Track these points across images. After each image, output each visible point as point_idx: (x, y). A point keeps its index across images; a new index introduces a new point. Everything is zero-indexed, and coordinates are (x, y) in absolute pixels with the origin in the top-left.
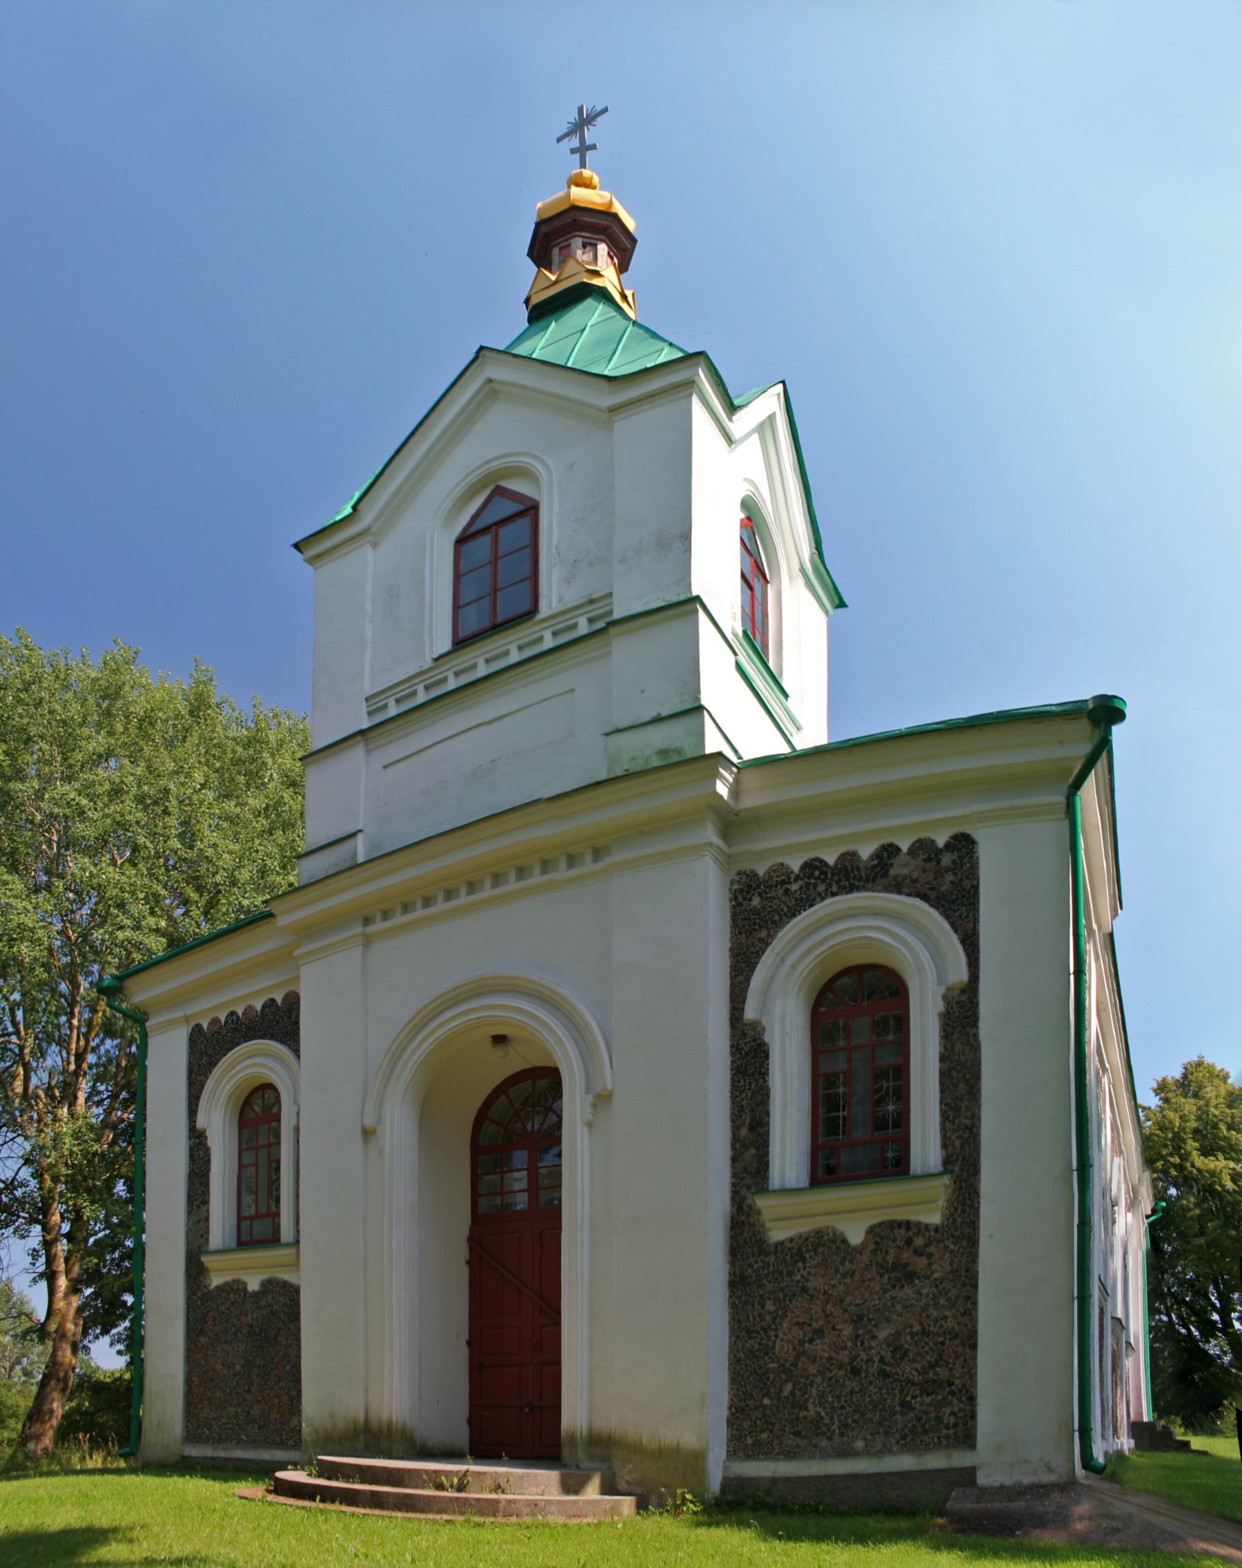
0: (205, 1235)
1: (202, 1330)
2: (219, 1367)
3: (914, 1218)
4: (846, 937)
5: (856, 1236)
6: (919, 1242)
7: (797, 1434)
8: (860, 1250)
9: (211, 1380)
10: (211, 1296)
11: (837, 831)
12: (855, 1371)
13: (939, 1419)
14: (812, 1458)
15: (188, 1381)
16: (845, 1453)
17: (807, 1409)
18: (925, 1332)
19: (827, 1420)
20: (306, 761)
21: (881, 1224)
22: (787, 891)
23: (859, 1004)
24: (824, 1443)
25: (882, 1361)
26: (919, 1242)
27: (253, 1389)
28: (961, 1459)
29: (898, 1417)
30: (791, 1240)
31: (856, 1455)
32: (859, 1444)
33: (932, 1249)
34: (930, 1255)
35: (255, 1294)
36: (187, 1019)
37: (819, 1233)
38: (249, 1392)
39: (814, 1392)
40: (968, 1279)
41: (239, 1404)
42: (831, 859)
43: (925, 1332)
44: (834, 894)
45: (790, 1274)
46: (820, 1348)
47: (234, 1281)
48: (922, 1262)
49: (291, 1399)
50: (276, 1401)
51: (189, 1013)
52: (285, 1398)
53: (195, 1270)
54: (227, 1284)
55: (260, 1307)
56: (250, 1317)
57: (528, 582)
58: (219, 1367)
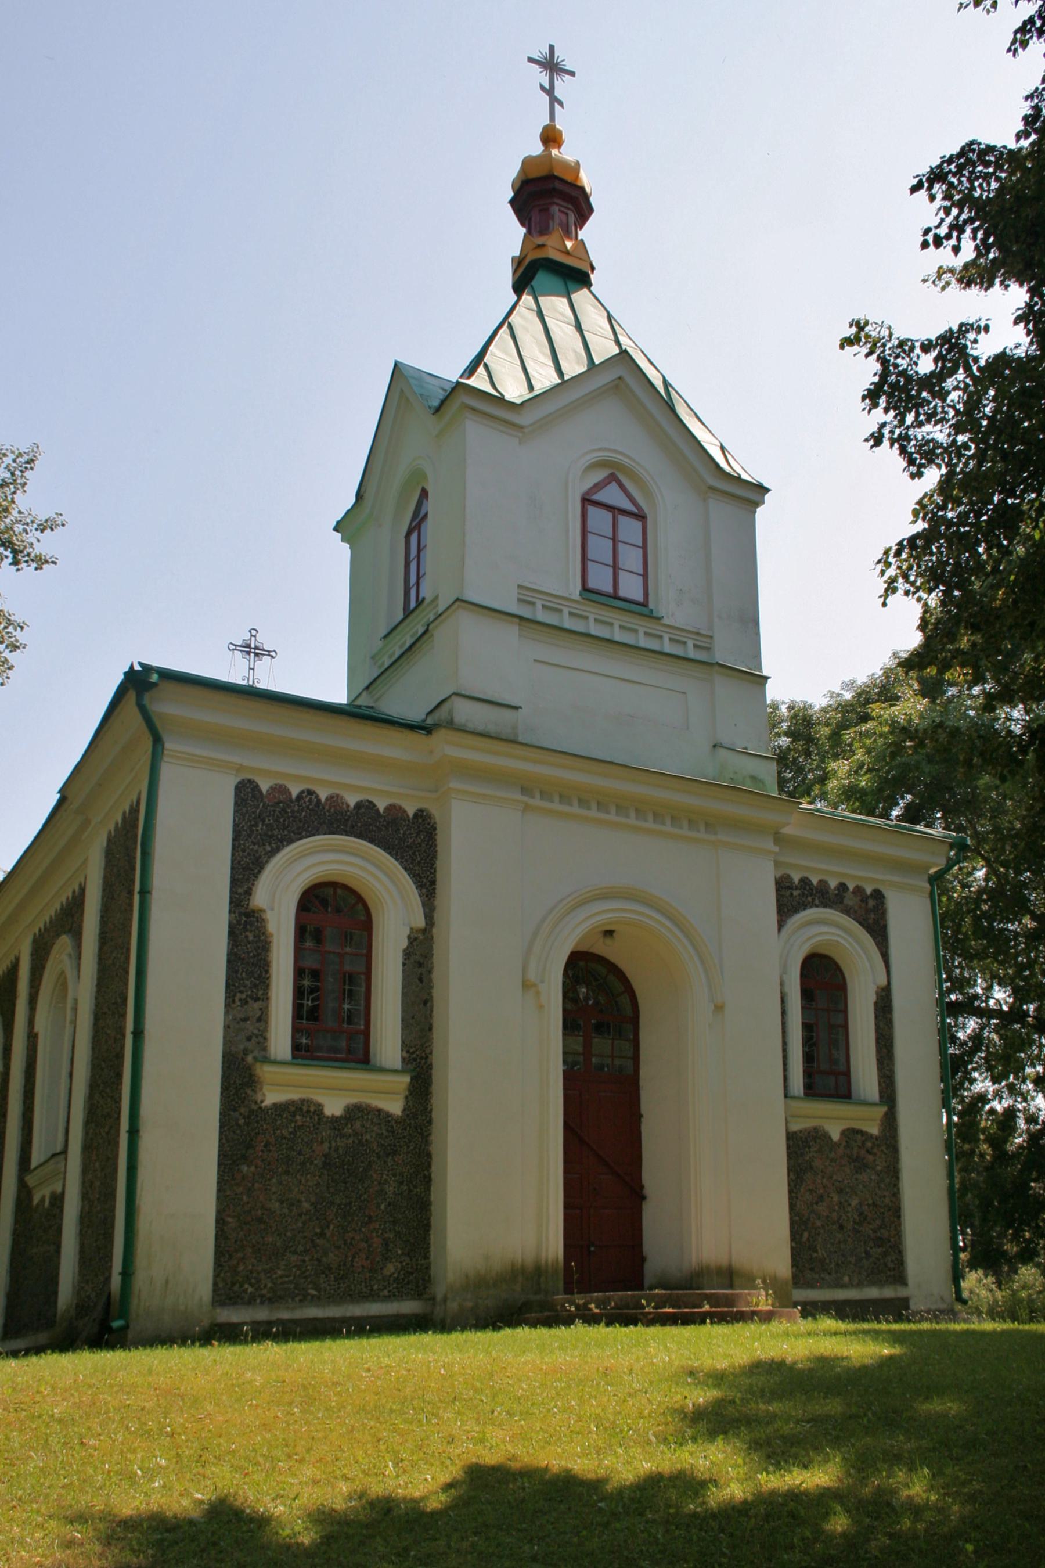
0: (261, 1038)
1: (244, 1157)
2: (275, 1206)
3: (864, 1129)
4: (827, 937)
5: (836, 1136)
6: (869, 1144)
7: (812, 1269)
8: (837, 1145)
9: (260, 1220)
10: (260, 1114)
11: (823, 866)
12: (841, 1227)
13: (886, 1265)
14: (821, 1287)
15: (220, 1221)
16: (839, 1285)
17: (816, 1251)
18: (874, 1204)
19: (827, 1261)
20: (371, 689)
21: (848, 1129)
22: (792, 894)
23: (333, 914)
24: (827, 1277)
25: (854, 1222)
26: (869, 1144)
27: (328, 1233)
28: (901, 1292)
29: (864, 1261)
30: (801, 1131)
31: (843, 1286)
32: (846, 1279)
33: (875, 1150)
34: (875, 1154)
35: (334, 1119)
36: (240, 768)
37: (816, 1129)
38: (322, 1235)
39: (820, 1240)
40: (893, 1172)
41: (306, 1251)
42: (815, 881)
43: (874, 1204)
44: (817, 906)
45: (802, 1155)
46: (822, 1208)
47: (303, 1101)
48: (871, 1158)
49: (314, 1014)
50: (364, 1245)
51: (246, 763)
52: (377, 1241)
53: (238, 1076)
54: (293, 1102)
55: (342, 1136)
56: (326, 1145)
57: (609, 589)
58: (275, 1206)
